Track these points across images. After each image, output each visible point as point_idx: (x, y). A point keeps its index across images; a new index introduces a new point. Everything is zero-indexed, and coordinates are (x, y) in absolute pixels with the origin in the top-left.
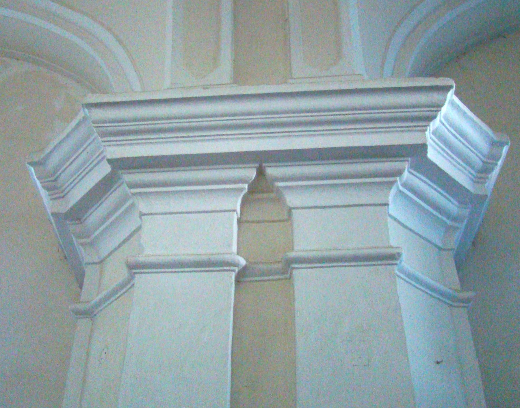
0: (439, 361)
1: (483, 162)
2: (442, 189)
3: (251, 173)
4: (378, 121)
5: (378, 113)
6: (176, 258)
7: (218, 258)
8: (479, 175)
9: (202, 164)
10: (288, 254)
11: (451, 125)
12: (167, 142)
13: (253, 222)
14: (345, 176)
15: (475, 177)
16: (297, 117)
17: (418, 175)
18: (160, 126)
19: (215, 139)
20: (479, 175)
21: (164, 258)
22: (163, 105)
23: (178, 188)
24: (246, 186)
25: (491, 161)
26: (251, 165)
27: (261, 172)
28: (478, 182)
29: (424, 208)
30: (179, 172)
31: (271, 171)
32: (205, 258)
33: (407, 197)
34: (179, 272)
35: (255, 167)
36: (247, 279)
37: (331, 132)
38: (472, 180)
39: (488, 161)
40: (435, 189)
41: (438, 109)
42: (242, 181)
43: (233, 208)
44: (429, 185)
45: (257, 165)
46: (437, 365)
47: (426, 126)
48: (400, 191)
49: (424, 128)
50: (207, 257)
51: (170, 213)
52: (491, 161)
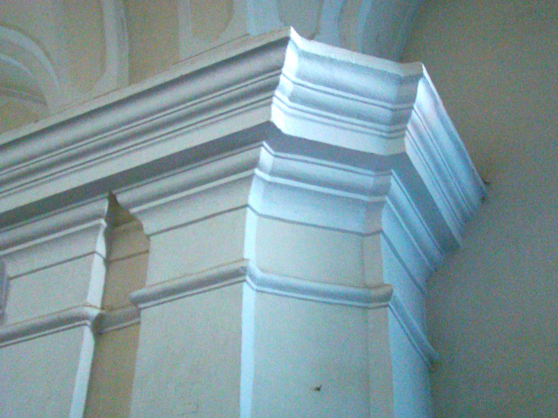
0: (318, 386)
1: (392, 110)
2: (337, 162)
3: (104, 206)
4: (95, 149)
5: (174, 112)
6: (29, 323)
7: (68, 313)
8: (393, 128)
9: (174, 167)
10: (131, 294)
11: (315, 82)
12: (100, 163)
13: (123, 259)
14: (227, 174)
15: (386, 132)
16: (212, 98)
17: (289, 155)
18: (112, 138)
19: (214, 121)
20: (393, 128)
21: (19, 325)
22: (9, 151)
23: (38, 241)
24: (103, 222)
25: (404, 106)
26: (101, 196)
27: (113, 200)
28: (391, 138)
29: (315, 192)
30: (148, 184)
31: (123, 198)
32: (55, 317)
33: (282, 186)
34: (35, 338)
35: (106, 197)
36: (109, 329)
37: (83, 166)
38: (384, 137)
39: (398, 106)
40: (328, 166)
41: (278, 72)
42: (98, 217)
43: (91, 251)
44: (313, 163)
45: (107, 194)
46: (317, 392)
47: (271, 97)
48: (270, 183)
49: (268, 101)
50: (56, 316)
51: (70, 260)
52: (404, 106)
